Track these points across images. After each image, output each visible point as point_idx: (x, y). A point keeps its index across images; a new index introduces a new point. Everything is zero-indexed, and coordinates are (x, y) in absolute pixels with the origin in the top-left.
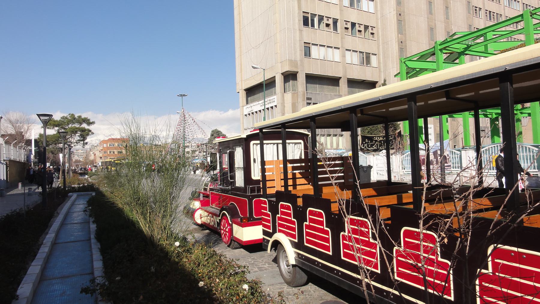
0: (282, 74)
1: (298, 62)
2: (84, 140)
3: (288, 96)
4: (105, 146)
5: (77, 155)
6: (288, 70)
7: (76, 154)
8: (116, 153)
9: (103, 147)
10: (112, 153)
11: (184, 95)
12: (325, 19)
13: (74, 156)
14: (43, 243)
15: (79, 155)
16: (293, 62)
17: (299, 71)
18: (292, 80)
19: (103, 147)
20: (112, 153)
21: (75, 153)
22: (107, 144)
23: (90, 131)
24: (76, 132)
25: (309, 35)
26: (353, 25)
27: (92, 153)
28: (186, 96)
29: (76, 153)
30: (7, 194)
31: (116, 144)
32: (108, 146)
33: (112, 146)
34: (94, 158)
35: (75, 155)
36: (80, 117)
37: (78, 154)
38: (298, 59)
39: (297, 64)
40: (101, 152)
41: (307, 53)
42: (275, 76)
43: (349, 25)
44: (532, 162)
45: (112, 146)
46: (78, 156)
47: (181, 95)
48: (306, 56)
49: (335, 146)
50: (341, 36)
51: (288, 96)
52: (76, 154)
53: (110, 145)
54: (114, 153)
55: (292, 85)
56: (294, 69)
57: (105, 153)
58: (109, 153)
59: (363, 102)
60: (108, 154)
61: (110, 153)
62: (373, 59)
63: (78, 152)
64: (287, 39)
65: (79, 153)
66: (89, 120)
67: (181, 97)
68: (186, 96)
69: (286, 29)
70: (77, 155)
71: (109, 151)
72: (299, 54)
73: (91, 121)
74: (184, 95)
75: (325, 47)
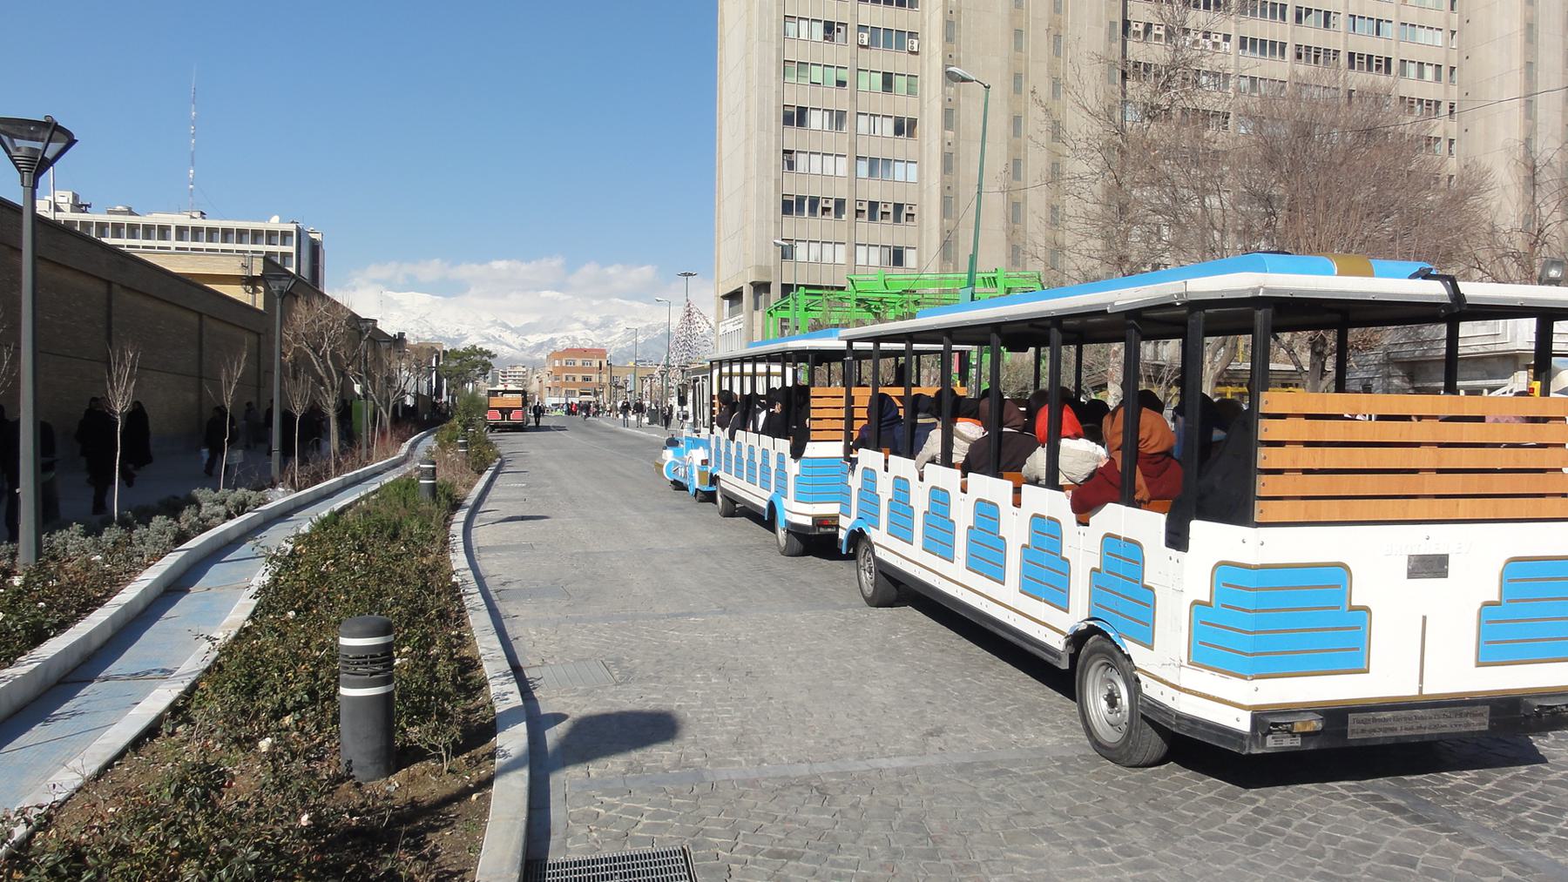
0: (752, 284)
2: (485, 374)
3: (758, 315)
9: (554, 367)
10: (570, 379)
12: (1155, 27)
14: (461, 504)
16: (759, 269)
17: (772, 280)
19: (554, 367)
20: (570, 379)
21: (508, 374)
22: (560, 359)
23: (491, 365)
25: (796, 226)
26: (873, 205)
31: (579, 363)
32: (564, 364)
37: (515, 376)
41: (787, 253)
43: (865, 207)
46: (515, 380)
47: (685, 274)
53: (567, 364)
54: (574, 379)
56: (765, 279)
57: (556, 379)
58: (564, 380)
59: (1275, 293)
61: (567, 379)
62: (910, 258)
63: (515, 372)
65: (517, 374)
71: (564, 375)
72: (773, 256)
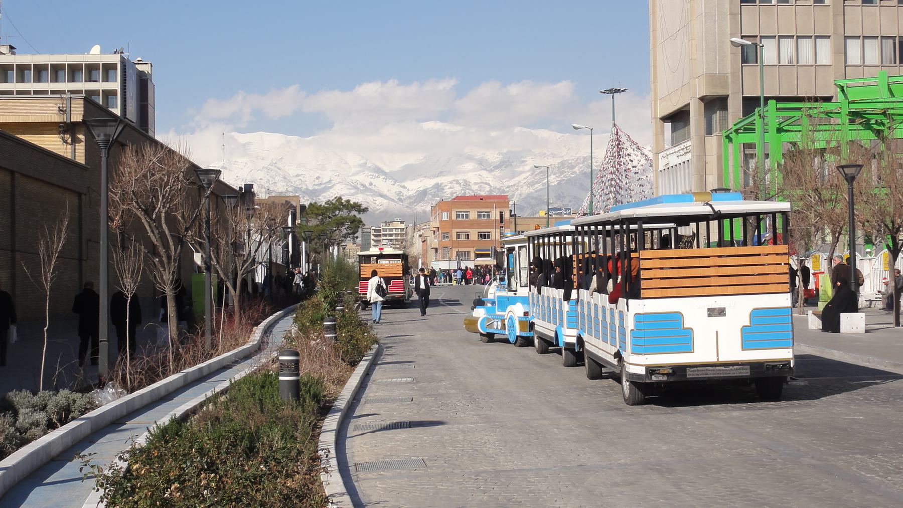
1: (727, 77)
4: (445, 216)
5: (388, 238)
6: (705, 95)
7: (385, 235)
8: (474, 237)
10: (463, 237)
11: (618, 91)
13: (380, 241)
15: (394, 237)
17: (730, 93)
18: (720, 110)
19: (441, 222)
20: (463, 237)
22: (449, 211)
24: (343, 224)
27: (417, 235)
28: (623, 91)
29: (385, 230)
30: (44, 482)
31: (473, 215)
32: (454, 217)
33: (463, 217)
34: (424, 250)
35: (383, 238)
36: (348, 201)
37: (391, 235)
38: (729, 70)
39: (726, 81)
40: (437, 233)
42: (689, 103)
44: (531, 261)
45: (463, 217)
48: (748, 63)
49: (714, 238)
50: (833, 13)
51: (712, 141)
52: (385, 235)
53: (458, 216)
54: (468, 236)
55: (720, 120)
56: (719, 92)
58: (454, 238)
60: (453, 242)
61: (458, 236)
64: (704, 34)
65: (394, 232)
66: (360, 206)
67: (612, 94)
68: (623, 91)
69: (703, 14)
70: (388, 238)
71: (454, 231)
72: (730, 60)
73: (363, 207)
74: (618, 91)
75: (793, 38)
